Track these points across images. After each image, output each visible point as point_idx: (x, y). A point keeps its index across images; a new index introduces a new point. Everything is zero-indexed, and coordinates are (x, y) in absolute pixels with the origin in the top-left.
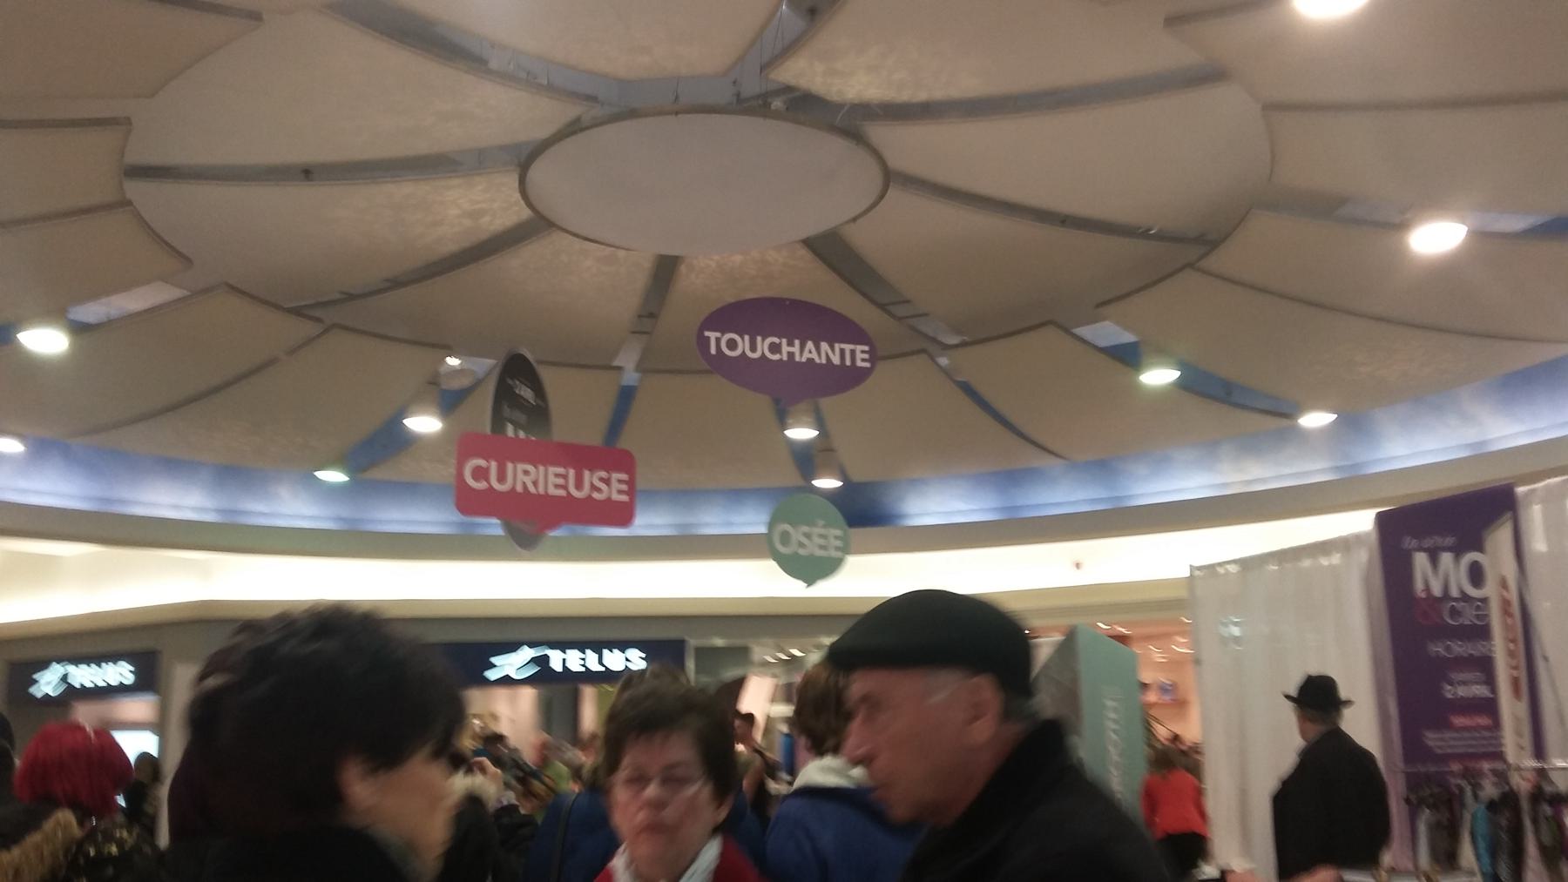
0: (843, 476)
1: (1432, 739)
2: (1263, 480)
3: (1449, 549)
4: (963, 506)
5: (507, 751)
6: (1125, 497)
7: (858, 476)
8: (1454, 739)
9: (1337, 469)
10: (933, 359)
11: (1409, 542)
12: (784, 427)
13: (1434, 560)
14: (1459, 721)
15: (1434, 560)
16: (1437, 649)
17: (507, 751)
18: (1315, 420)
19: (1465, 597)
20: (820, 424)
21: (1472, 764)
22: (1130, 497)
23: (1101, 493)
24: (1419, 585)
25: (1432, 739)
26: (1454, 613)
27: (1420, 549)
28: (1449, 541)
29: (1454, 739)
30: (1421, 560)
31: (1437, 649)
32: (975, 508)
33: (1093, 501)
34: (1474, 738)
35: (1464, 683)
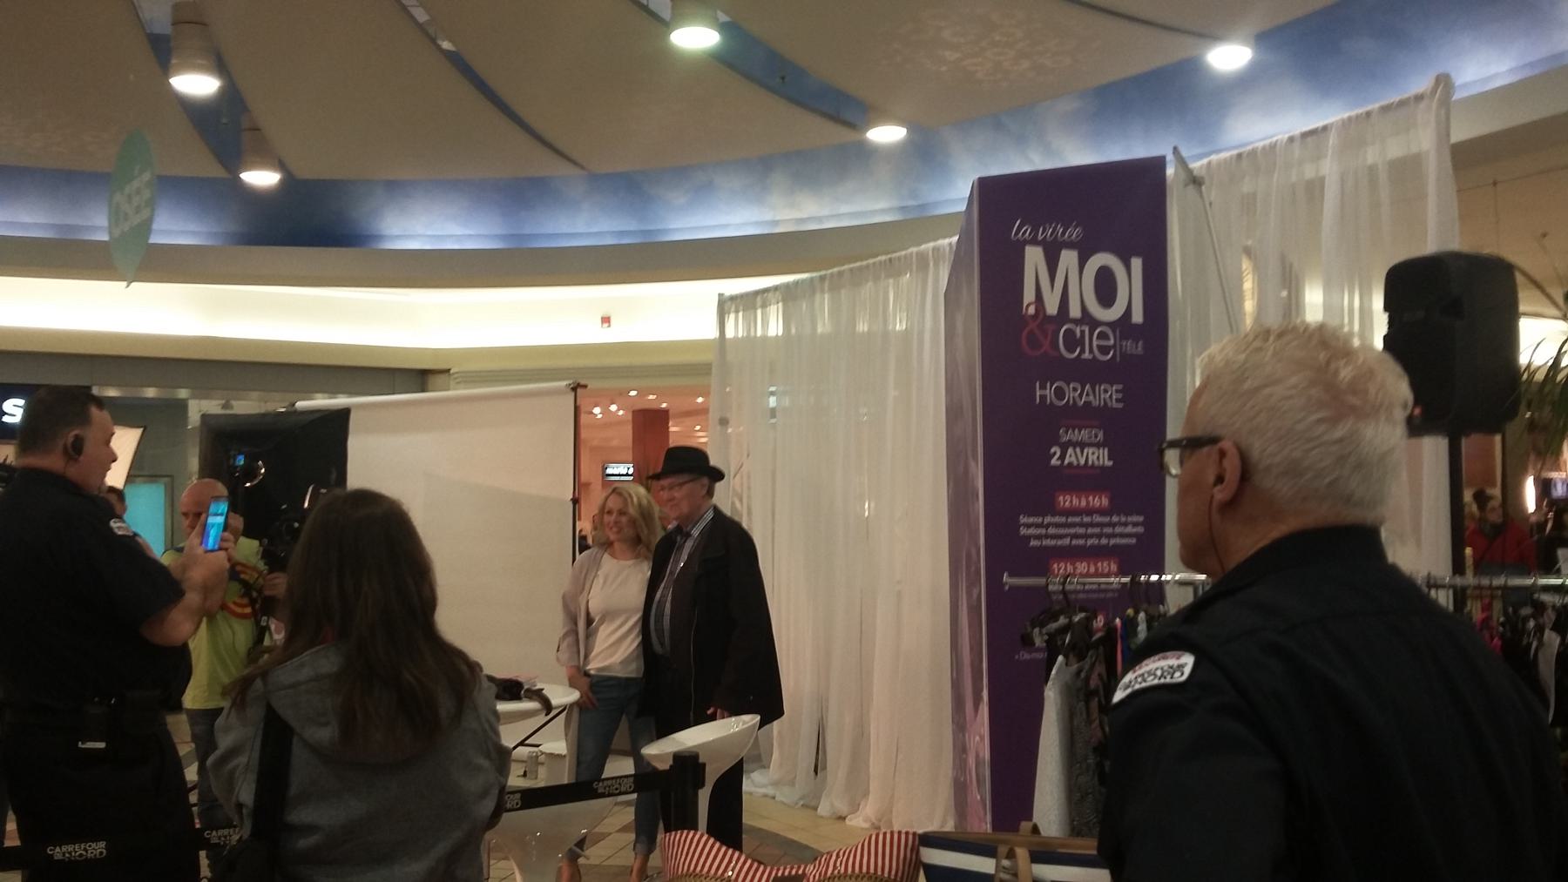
0: (281, 166)
1: (1029, 526)
2: (819, 219)
3: (1070, 245)
4: (456, 230)
5: (1468, 551)
6: (659, 230)
7: (306, 171)
8: (1057, 525)
9: (903, 209)
10: (433, 41)
11: (1021, 230)
12: (166, 69)
13: (1052, 263)
14: (1066, 501)
15: (1052, 263)
16: (1046, 392)
17: (1468, 551)
18: (887, 134)
19: (1087, 318)
20: (219, 66)
21: (606, 511)
22: (666, 231)
23: (630, 225)
24: (1029, 296)
25: (1029, 526)
26: (1072, 342)
27: (1034, 242)
28: (1074, 233)
29: (1057, 525)
30: (1034, 257)
31: (1046, 392)
32: (472, 233)
33: (622, 233)
34: (1081, 525)
35: (1082, 445)
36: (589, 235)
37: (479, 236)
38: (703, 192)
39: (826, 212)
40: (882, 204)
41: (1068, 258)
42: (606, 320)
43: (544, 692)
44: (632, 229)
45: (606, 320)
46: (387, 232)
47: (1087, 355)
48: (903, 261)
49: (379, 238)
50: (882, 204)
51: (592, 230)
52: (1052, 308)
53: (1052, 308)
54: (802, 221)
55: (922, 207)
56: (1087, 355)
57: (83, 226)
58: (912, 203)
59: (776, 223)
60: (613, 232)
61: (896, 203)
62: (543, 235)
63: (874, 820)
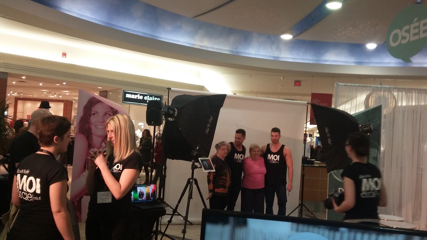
9: (232, 51)
28: (28, 172)
32: (93, 17)
33: (145, 33)
36: (134, 31)
37: (95, 19)
38: (177, 29)
39: (210, 46)
40: (227, 48)
41: (239, 154)
42: (64, 55)
43: (84, 172)
44: (148, 33)
45: (64, 55)
46: (62, 7)
47: (273, 163)
48: (386, 88)
49: (60, 8)
50: (227, 48)
51: (135, 30)
52: (237, 158)
53: (237, 158)
54: (201, 46)
55: (238, 52)
56: (273, 163)
57: (156, 36)
58: (235, 50)
59: (194, 45)
60: (142, 32)
61: (230, 49)
62: (129, 29)
63: (247, 143)
